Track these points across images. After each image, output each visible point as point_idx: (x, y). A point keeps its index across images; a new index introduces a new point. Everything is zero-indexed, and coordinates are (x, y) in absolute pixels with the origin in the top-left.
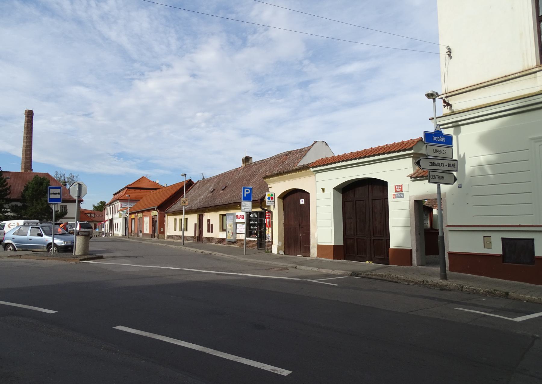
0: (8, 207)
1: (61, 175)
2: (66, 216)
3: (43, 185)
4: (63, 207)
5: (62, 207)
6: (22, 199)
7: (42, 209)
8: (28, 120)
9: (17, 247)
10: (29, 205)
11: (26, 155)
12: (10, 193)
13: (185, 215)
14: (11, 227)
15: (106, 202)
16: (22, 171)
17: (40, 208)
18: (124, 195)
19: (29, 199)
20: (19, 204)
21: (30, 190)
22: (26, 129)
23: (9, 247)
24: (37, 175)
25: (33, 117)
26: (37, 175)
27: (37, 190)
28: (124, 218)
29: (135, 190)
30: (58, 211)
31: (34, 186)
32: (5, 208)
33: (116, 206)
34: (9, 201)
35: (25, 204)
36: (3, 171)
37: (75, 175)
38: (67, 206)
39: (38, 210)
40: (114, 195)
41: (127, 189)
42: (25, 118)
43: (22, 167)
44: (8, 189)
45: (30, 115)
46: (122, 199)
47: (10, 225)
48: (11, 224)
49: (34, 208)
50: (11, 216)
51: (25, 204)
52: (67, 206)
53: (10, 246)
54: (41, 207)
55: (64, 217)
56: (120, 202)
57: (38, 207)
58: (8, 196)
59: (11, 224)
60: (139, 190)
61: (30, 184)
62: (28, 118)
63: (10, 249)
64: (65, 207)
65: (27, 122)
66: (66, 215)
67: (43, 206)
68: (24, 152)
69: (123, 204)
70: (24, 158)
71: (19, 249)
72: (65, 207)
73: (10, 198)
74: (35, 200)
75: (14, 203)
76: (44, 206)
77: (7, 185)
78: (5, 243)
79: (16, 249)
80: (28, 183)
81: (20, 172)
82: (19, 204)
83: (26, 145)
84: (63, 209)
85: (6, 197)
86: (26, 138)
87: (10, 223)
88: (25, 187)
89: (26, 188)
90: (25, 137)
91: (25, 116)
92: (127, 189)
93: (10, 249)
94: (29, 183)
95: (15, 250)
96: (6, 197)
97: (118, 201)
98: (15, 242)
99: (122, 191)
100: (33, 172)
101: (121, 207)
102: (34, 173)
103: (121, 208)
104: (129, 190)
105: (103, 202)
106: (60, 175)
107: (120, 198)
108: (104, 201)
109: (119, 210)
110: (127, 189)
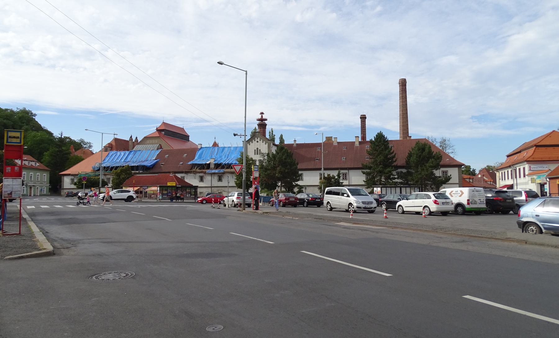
0: (395, 174)
1: (433, 140)
2: (450, 182)
3: (426, 151)
4: (444, 173)
5: (443, 172)
6: (407, 166)
7: (427, 175)
8: (402, 88)
9: (545, 228)
10: (414, 172)
11: (403, 123)
12: (396, 160)
13: (512, 183)
14: (453, 195)
15: (471, 166)
16: (401, 139)
17: (425, 174)
18: (532, 155)
19: (414, 165)
20: (404, 171)
21: (415, 157)
22: (401, 98)
23: (530, 228)
24: (418, 142)
25: (407, 85)
26: (419, 141)
27: (420, 156)
28: (538, 183)
29: (546, 148)
30: (441, 176)
31: (417, 152)
32: (393, 175)
33: (520, 169)
34: (397, 167)
35: (410, 170)
36: (389, 140)
37: (446, 139)
38: (448, 171)
39: (423, 176)
40: (508, 156)
41: (536, 148)
42: (400, 87)
43: (400, 135)
44: (394, 157)
45: (404, 83)
46: (530, 160)
47: (452, 194)
48: (454, 192)
49: (419, 174)
50: (399, 182)
51: (410, 170)
52: (448, 171)
53: (531, 227)
54: (426, 173)
55: (448, 183)
56: (529, 164)
57: (423, 173)
58: (395, 164)
59: (454, 192)
60: (552, 148)
61: (414, 151)
62: (402, 87)
63: (533, 231)
64: (446, 172)
65: (402, 91)
66: (450, 180)
67: (428, 172)
68: (401, 121)
69: (532, 166)
70: (401, 126)
71: (547, 231)
72: (446, 172)
73: (397, 165)
74: (420, 165)
75: (399, 170)
76: (429, 172)
77: (393, 153)
78: (522, 221)
79: (544, 231)
80: (411, 150)
81: (399, 139)
82: (404, 171)
83: (402, 113)
84: (444, 175)
85: (393, 165)
86: (402, 106)
87: (452, 192)
88: (408, 153)
89: (410, 155)
90: (401, 106)
91: (399, 86)
92: (535, 147)
93: (533, 231)
94: (413, 149)
95: (541, 232)
96: (393, 165)
97: (526, 163)
98: (541, 221)
99: (523, 151)
100: (412, 139)
101: (530, 170)
102: (413, 139)
103: (530, 172)
104: (538, 149)
105: (468, 166)
106: (432, 140)
107: (527, 159)
108: (469, 165)
109: (527, 173)
110: (535, 147)
